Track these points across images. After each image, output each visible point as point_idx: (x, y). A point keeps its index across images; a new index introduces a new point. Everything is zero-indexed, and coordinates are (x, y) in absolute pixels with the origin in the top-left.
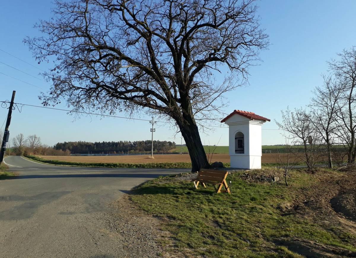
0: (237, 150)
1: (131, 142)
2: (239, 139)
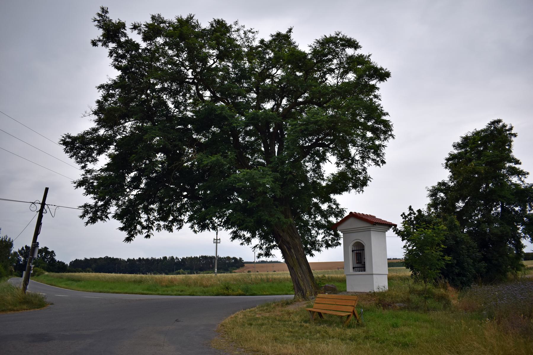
0: (355, 267)
1: (179, 258)
2: (357, 252)
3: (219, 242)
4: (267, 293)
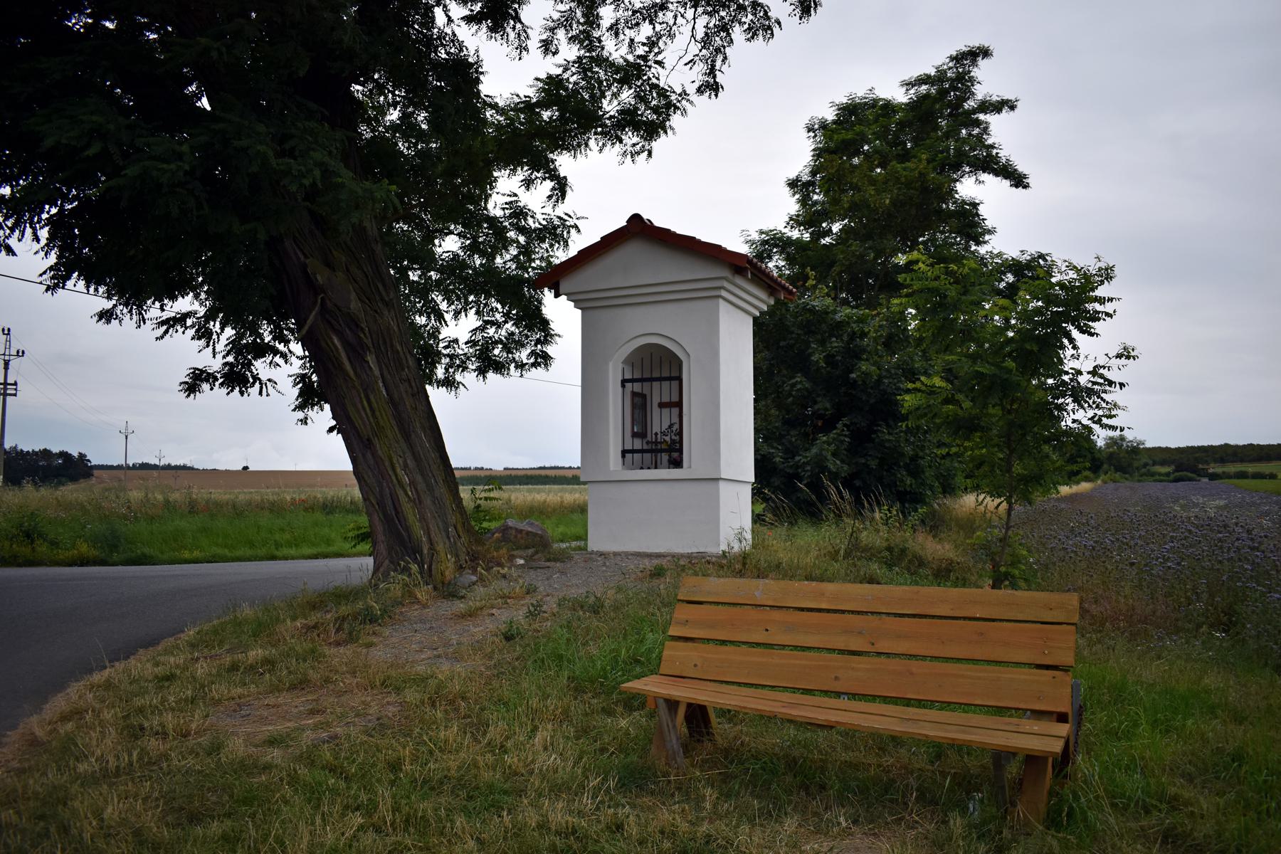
3: (14, 392)
4: (196, 554)
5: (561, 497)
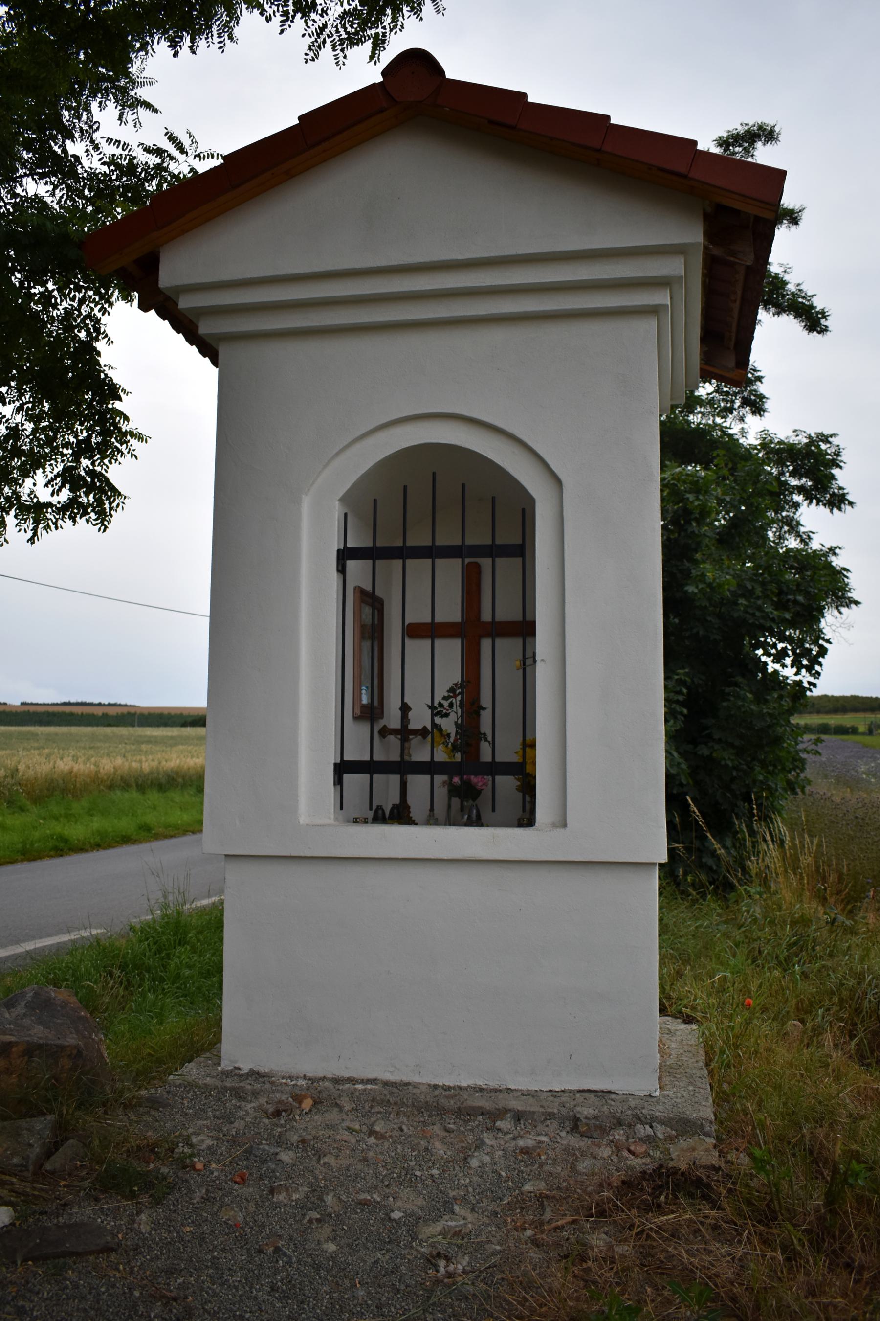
5: (96, 764)
